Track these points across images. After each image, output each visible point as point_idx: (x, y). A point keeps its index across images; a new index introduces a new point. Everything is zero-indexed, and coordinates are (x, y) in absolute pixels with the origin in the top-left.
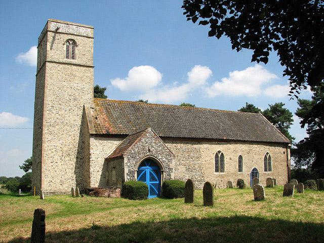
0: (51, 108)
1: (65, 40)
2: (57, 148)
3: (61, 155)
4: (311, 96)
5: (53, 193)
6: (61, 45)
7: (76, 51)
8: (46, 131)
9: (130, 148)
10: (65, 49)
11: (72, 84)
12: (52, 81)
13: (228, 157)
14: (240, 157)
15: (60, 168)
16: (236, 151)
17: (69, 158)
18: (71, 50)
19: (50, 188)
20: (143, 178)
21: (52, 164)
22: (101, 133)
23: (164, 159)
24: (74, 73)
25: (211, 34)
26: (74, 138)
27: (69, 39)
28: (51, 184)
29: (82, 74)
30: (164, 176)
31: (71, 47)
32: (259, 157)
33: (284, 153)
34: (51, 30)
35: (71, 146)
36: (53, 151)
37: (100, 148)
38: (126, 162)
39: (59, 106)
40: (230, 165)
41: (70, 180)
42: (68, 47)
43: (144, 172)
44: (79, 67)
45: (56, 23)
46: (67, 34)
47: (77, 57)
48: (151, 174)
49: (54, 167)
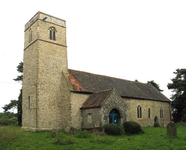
1: (49, 27)
3: (49, 104)
4: (154, 80)
6: (46, 30)
7: (56, 35)
9: (105, 101)
10: (49, 33)
12: (42, 53)
13: (144, 109)
14: (149, 109)
16: (147, 106)
17: (54, 107)
18: (52, 34)
20: (111, 121)
21: (44, 110)
24: (55, 49)
25: (17, 70)
28: (43, 124)
34: (40, 18)
35: (55, 99)
42: (51, 32)
43: (111, 117)
44: (58, 46)
45: (43, 15)
47: (57, 39)
49: (45, 112)
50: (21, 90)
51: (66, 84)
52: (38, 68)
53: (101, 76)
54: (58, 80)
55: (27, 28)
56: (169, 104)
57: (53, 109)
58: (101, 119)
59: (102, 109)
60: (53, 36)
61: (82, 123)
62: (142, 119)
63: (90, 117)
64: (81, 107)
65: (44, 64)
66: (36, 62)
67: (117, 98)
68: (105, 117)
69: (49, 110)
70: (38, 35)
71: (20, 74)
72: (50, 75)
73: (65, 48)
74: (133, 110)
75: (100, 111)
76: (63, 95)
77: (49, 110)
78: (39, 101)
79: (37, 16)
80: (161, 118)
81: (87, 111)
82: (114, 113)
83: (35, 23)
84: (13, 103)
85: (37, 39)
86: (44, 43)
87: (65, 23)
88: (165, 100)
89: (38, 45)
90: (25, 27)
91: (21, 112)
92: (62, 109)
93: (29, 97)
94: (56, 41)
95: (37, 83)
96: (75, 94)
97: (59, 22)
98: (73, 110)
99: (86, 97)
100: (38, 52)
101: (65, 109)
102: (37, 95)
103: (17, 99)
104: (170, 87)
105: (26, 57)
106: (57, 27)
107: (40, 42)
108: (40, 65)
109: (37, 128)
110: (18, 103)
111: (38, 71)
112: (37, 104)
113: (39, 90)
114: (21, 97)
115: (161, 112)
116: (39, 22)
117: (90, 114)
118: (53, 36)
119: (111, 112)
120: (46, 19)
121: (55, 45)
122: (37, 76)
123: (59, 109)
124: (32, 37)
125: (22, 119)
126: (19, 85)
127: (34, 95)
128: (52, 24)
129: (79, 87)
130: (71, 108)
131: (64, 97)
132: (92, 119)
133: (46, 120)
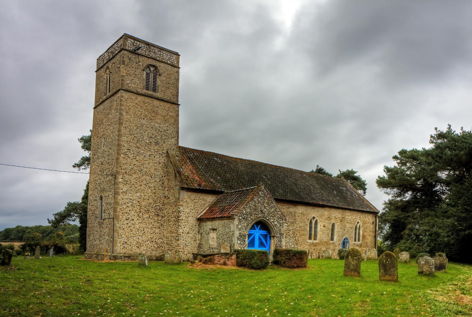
0: (126, 151)
1: (144, 65)
2: (134, 202)
3: (138, 210)
5: (129, 257)
6: (138, 71)
7: (158, 82)
8: (121, 180)
10: (144, 76)
11: (152, 124)
12: (129, 117)
13: (322, 225)
14: (333, 225)
15: (137, 226)
17: (148, 216)
18: (151, 80)
19: (124, 251)
20: (252, 243)
22: (193, 187)
23: (276, 223)
26: (154, 191)
27: (151, 65)
28: (126, 246)
29: (165, 113)
30: (276, 241)
31: (152, 75)
32: (351, 226)
33: (373, 223)
35: (151, 201)
36: (129, 205)
37: (191, 205)
38: (237, 223)
39: (137, 149)
40: (322, 234)
41: (149, 242)
42: (148, 74)
44: (162, 103)
46: (147, 57)
47: (160, 90)
48: (260, 239)
49: (130, 224)
50: (88, 182)
51: (174, 175)
52: (119, 145)
53: (245, 160)
54: (159, 167)
55: (102, 65)
56: (376, 217)
57: (146, 219)
58: (233, 239)
59: (236, 222)
60: (151, 85)
61: (200, 246)
62: (317, 241)
63: (213, 235)
64: (199, 216)
65: (133, 136)
66: (117, 133)
67: (268, 203)
68: (241, 236)
69: (138, 222)
70: (122, 80)
71: (86, 154)
72: (142, 157)
73: (175, 106)
74: (301, 225)
75: (232, 226)
76: (166, 194)
77: (138, 222)
78: (119, 205)
79: (121, 42)
80: (355, 241)
81: (209, 225)
82: (260, 230)
83: (118, 57)
84: (72, 208)
85: (120, 90)
86: (134, 97)
87: (179, 58)
88: (368, 210)
89: (121, 100)
90: (98, 64)
91: (86, 226)
92: (163, 219)
93: (101, 198)
94: (158, 94)
95: (117, 172)
96: (189, 194)
97: (166, 57)
98: (183, 221)
99: (210, 199)
100: (121, 114)
101: (169, 221)
102: (116, 193)
103: (80, 201)
104: (382, 183)
105: (97, 123)
106: (162, 67)
107: (126, 95)
108: (124, 138)
109: (113, 253)
110: (80, 209)
111: (119, 150)
112: (115, 211)
113: (121, 186)
114: (85, 198)
115: (357, 231)
116: (125, 55)
117: (214, 230)
118: (151, 85)
119: (253, 228)
120: (138, 49)
121: (156, 103)
122: (117, 159)
123: (158, 220)
124: (111, 84)
125: (87, 237)
126: (84, 176)
127: (111, 194)
128: (150, 59)
129: (196, 180)
130: (180, 218)
131: (169, 198)
132: (217, 238)
133: (131, 240)
